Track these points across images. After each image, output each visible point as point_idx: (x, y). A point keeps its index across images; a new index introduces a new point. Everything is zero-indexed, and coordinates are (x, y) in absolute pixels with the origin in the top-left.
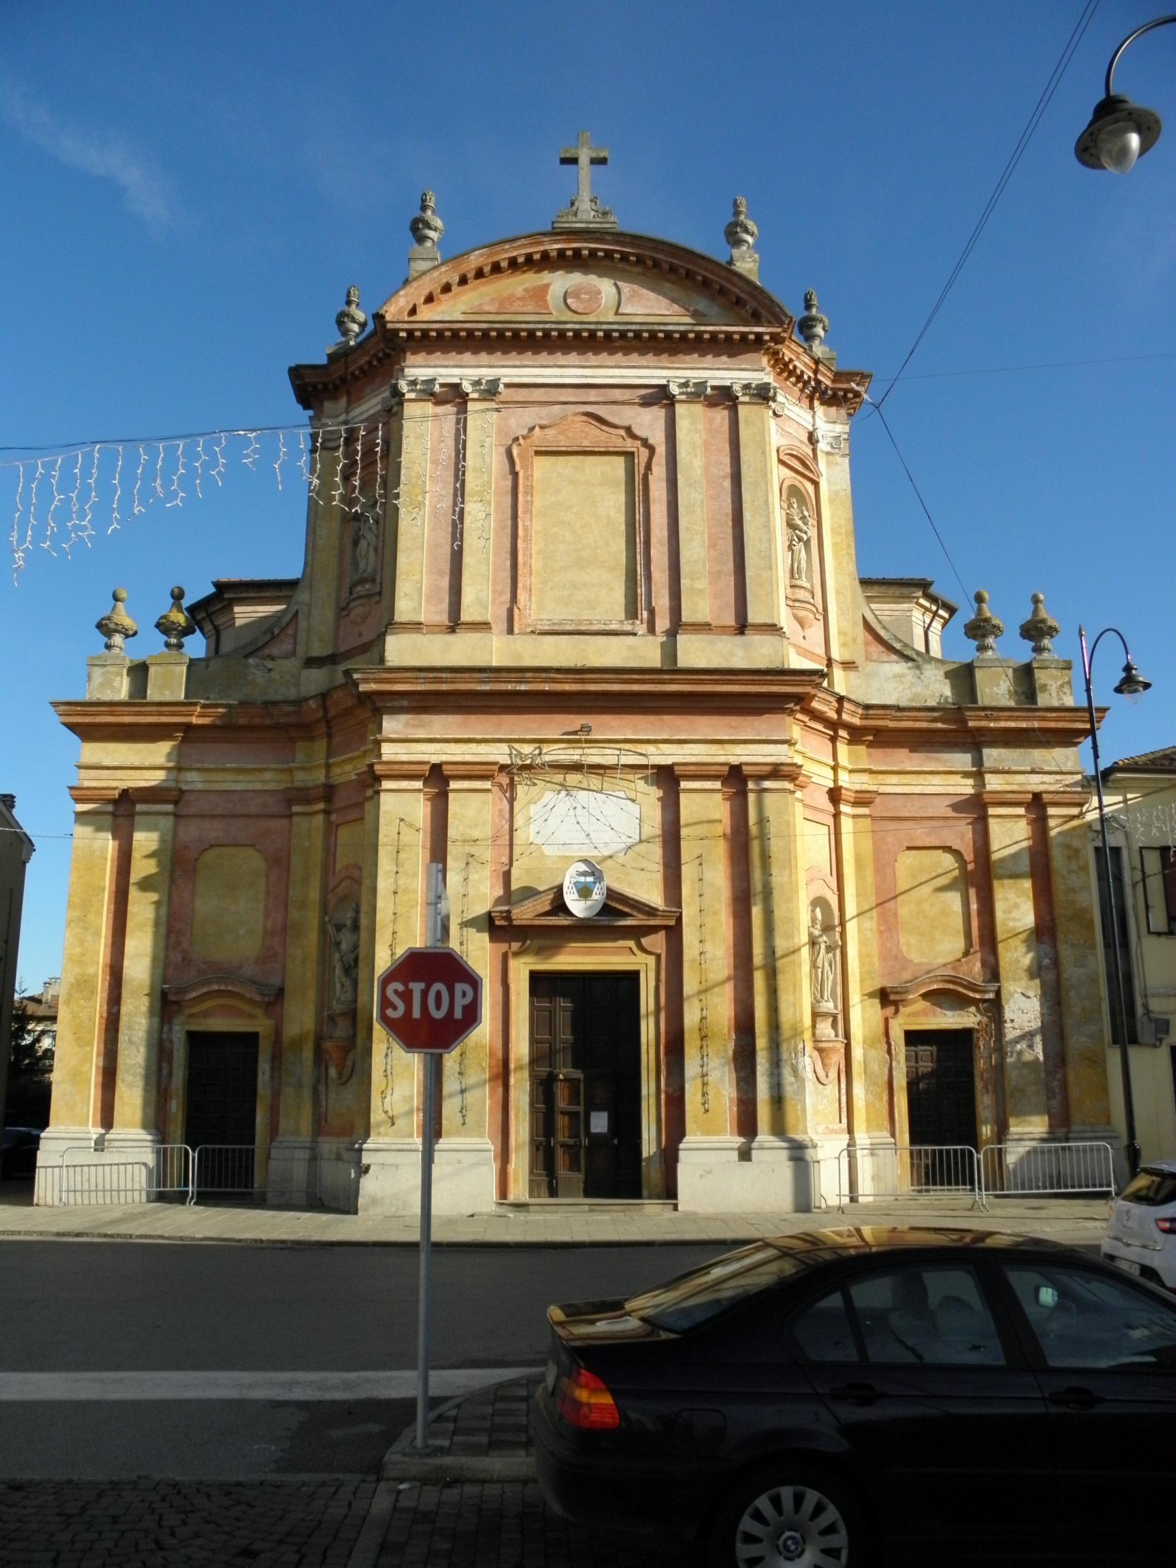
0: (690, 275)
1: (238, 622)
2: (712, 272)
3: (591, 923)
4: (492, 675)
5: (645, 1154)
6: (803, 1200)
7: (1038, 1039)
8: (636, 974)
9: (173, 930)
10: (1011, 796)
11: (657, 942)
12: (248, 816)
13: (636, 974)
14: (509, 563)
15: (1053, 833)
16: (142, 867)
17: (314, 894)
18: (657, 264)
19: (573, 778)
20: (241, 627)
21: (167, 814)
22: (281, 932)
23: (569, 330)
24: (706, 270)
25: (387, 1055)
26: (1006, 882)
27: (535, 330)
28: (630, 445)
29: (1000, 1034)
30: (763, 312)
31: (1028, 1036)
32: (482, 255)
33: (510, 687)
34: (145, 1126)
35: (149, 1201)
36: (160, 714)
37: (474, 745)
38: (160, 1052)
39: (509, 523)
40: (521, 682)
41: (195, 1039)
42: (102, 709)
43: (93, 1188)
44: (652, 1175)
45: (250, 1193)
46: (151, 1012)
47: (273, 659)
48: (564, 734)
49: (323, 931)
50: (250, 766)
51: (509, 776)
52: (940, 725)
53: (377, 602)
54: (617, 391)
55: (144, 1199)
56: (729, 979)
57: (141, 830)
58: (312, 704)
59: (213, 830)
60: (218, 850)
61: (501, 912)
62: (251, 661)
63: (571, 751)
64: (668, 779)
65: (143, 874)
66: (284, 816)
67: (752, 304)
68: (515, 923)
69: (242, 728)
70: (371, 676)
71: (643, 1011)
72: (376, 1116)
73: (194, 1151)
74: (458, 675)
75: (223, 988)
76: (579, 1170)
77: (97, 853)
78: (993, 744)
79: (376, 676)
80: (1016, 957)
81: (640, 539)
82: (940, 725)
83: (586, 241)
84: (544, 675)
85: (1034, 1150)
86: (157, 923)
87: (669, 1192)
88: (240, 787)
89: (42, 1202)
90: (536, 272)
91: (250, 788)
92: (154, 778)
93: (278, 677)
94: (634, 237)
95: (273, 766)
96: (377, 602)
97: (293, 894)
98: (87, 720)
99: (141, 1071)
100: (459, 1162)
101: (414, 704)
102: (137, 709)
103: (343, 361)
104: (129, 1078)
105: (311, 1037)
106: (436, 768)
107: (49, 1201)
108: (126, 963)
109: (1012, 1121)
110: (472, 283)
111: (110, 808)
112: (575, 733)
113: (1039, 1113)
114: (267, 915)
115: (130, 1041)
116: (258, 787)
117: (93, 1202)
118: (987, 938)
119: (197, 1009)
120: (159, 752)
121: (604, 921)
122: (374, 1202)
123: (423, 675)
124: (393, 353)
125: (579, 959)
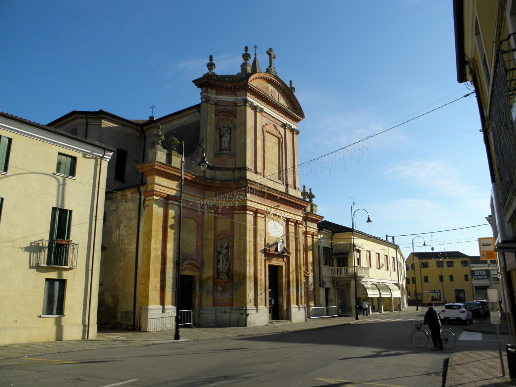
0: (290, 99)
1: (103, 126)
6: (59, 337)
11: (285, 259)
20: (103, 128)
21: (177, 205)
22: (201, 247)
28: (279, 136)
34: (172, 305)
44: (285, 314)
49: (215, 247)
64: (287, 220)
67: (298, 111)
69: (197, 184)
72: (248, 301)
81: (281, 161)
87: (289, 317)
92: (173, 193)
98: (163, 169)
105: (212, 278)
111: (163, 199)
122: (250, 323)
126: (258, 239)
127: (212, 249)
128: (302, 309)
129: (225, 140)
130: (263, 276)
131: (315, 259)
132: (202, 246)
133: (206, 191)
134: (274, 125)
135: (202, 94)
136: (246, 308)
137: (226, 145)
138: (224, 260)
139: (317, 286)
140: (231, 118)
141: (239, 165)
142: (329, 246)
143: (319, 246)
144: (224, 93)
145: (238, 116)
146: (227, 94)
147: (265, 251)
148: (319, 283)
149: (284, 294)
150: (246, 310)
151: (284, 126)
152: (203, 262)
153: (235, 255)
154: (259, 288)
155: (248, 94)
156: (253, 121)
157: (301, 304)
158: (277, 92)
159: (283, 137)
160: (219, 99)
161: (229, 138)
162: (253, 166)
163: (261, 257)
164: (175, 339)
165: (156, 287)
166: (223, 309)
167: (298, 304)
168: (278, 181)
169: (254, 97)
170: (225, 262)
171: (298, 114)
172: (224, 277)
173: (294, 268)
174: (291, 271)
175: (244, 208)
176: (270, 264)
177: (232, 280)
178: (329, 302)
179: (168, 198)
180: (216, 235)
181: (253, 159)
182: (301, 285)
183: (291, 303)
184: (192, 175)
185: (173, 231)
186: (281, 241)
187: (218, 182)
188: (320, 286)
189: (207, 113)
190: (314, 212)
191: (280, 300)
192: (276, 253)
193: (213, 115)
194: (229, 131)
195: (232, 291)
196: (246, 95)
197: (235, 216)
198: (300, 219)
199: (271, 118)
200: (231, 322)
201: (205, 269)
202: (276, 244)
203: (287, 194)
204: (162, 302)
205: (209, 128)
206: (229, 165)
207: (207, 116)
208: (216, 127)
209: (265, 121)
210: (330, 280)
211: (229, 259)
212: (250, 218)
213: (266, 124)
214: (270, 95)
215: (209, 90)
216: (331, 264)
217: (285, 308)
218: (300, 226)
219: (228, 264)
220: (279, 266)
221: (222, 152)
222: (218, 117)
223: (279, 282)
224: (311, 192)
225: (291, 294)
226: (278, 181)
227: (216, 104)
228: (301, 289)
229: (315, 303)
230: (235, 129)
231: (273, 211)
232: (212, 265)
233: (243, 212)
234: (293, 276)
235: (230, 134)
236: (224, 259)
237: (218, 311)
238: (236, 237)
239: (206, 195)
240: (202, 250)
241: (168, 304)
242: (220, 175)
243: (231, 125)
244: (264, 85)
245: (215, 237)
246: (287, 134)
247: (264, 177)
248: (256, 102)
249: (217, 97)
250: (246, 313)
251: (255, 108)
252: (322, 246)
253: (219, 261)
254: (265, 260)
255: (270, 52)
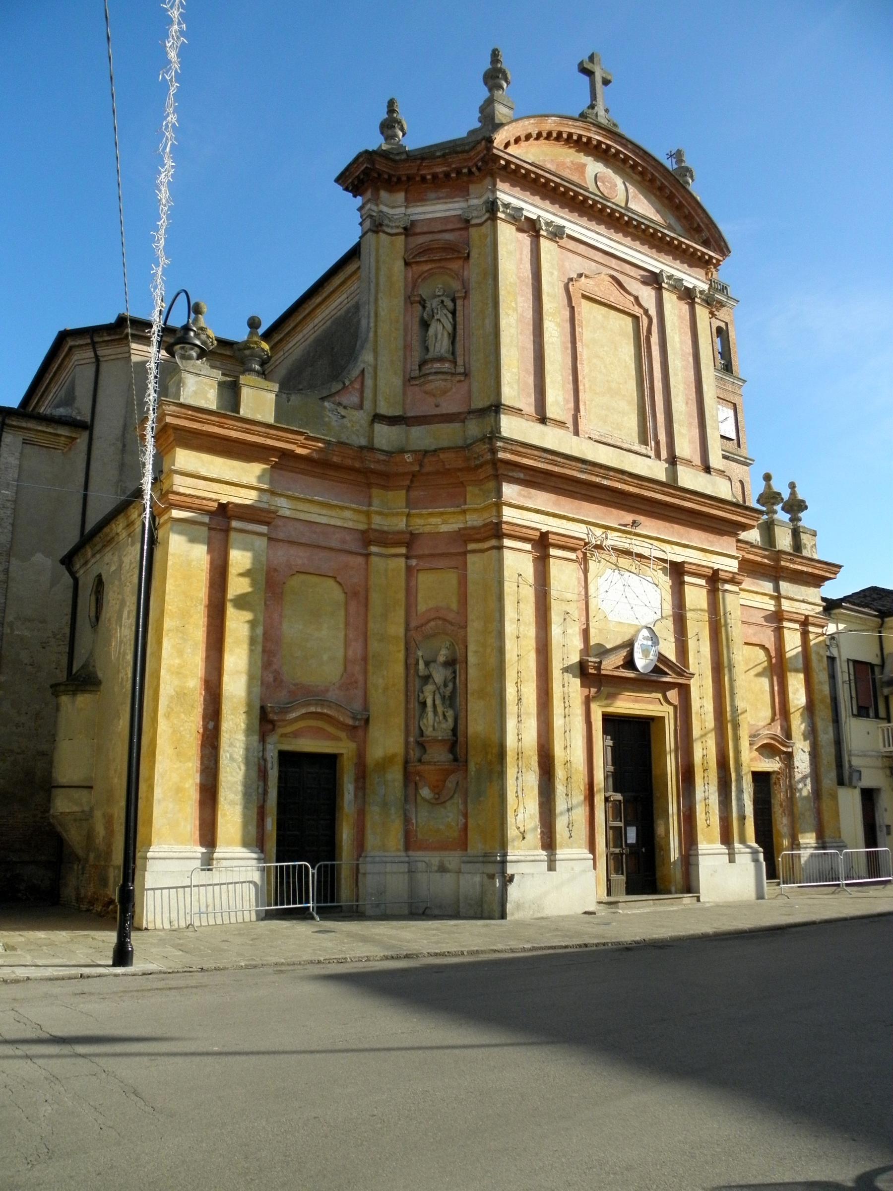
2: (686, 200)
3: (646, 678)
4: (589, 468)
5: (672, 860)
7: (808, 781)
8: (663, 718)
9: (267, 648)
10: (796, 615)
11: (673, 695)
12: (331, 549)
13: (663, 718)
14: (571, 378)
15: (812, 643)
16: (237, 586)
17: (397, 629)
18: (652, 180)
19: (624, 562)
22: (361, 664)
23: (609, 207)
24: (683, 197)
25: (517, 778)
26: (793, 674)
27: (588, 198)
28: (638, 311)
29: (791, 776)
30: (713, 242)
31: (804, 778)
32: (555, 122)
33: (598, 480)
34: (245, 844)
35: (258, 920)
36: (267, 436)
37: (564, 521)
38: (257, 770)
39: (569, 345)
40: (605, 478)
41: (285, 757)
42: (213, 418)
43: (203, 909)
44: (677, 874)
45: (341, 906)
46: (249, 731)
47: (345, 408)
48: (620, 525)
49: (409, 666)
50: (335, 502)
51: (584, 552)
52: (766, 561)
53: (460, 381)
54: (628, 266)
55: (254, 918)
56: (712, 730)
57: (239, 548)
58: (408, 458)
59: (300, 557)
60: (302, 577)
61: (595, 662)
62: (326, 404)
63: (624, 540)
65: (240, 591)
66: (361, 554)
67: (705, 234)
68: (603, 672)
70: (510, 447)
71: (668, 749)
72: (512, 832)
73: (313, 867)
74: (568, 462)
75: (319, 710)
76: (622, 874)
77: (194, 563)
78: (786, 579)
79: (514, 448)
80: (798, 726)
81: (646, 385)
82: (766, 561)
83: (615, 142)
84: (621, 476)
85: (812, 855)
86: (252, 641)
87: (690, 886)
88: (324, 520)
89: (151, 926)
90: (577, 151)
91: (332, 523)
92: (248, 497)
93: (349, 425)
94: (645, 152)
95: (354, 506)
96: (460, 381)
97: (373, 626)
99: (240, 788)
100: (573, 869)
101: (528, 478)
102: (247, 426)
103: (418, 162)
104: (231, 796)
105: (400, 760)
106: (544, 535)
107: (159, 925)
108: (226, 679)
109: (800, 836)
110: (542, 141)
111: (206, 519)
112: (625, 525)
113: (811, 831)
114: (347, 645)
115: (232, 759)
116: (339, 523)
117: (233, 920)
118: (782, 711)
119: (289, 729)
120: (251, 472)
121: (654, 677)
122: (518, 906)
123: (545, 455)
124: (477, 173)
125: (631, 705)
126: (556, 630)
127: (399, 669)
128: (744, 860)
129: (439, 332)
130: (580, 747)
131: (817, 697)
132: (365, 659)
133: (375, 492)
134: (613, 277)
135: (363, 212)
136: (505, 855)
137: (441, 345)
138: (438, 702)
139: (829, 778)
140: (455, 266)
141: (479, 403)
142: (869, 655)
143: (832, 659)
144: (432, 195)
145: (474, 255)
146: (439, 199)
147: (584, 671)
148: (833, 774)
149: (673, 808)
150: (504, 862)
151: (654, 280)
152: (366, 708)
153: (472, 686)
154: (560, 789)
155: (500, 185)
156: (528, 266)
157: (743, 841)
158: (619, 181)
159: (653, 312)
160: (412, 218)
161: (449, 327)
162: (532, 400)
163: (569, 691)
164: (115, 965)
165: (179, 790)
166: (434, 858)
167: (726, 838)
168: (642, 449)
169: (517, 191)
170: (440, 709)
171: (706, 243)
172: (439, 755)
173: (710, 723)
174: (696, 732)
175: (496, 532)
176: (610, 710)
177: (459, 764)
178: (881, 835)
179: (224, 511)
180: (413, 624)
181: (531, 380)
182: (739, 778)
183: (700, 837)
184: (308, 438)
185: (248, 616)
186: (645, 633)
187: (408, 458)
188: (841, 782)
189: (377, 261)
190: (805, 553)
191: (660, 830)
192: (630, 674)
193: (400, 264)
194: (450, 304)
195: (465, 803)
196: (494, 190)
197: (471, 558)
198: (732, 565)
199: (599, 257)
200: (458, 900)
201: (376, 731)
202: (629, 645)
203: (672, 485)
204: (208, 836)
205: (384, 304)
206: (449, 406)
207: (378, 269)
208: (409, 300)
209: (575, 265)
210: (879, 763)
211: (453, 698)
212: (517, 562)
213: (580, 275)
214: (592, 188)
215: (383, 194)
216: (882, 713)
217: (674, 854)
218: (727, 587)
219: (450, 713)
220: (652, 719)
221: (427, 369)
222: (415, 268)
223: (655, 771)
224: (793, 493)
225: (700, 808)
226: (637, 447)
227: (408, 231)
228: (740, 791)
229: (820, 836)
230: (465, 297)
231: (614, 539)
232: (399, 720)
233: (493, 542)
234: (705, 751)
235: (454, 313)
236: (438, 697)
237: (421, 866)
238: (474, 626)
239: (376, 502)
240: (365, 672)
241: (229, 843)
242: (421, 437)
243: (456, 285)
244: (568, 160)
245: (407, 629)
246: (667, 306)
247: (576, 433)
248: (534, 208)
249: (410, 211)
250: (503, 872)
251: (532, 228)
252: (844, 658)
253: (424, 704)
254: (587, 701)
255: (588, 66)
